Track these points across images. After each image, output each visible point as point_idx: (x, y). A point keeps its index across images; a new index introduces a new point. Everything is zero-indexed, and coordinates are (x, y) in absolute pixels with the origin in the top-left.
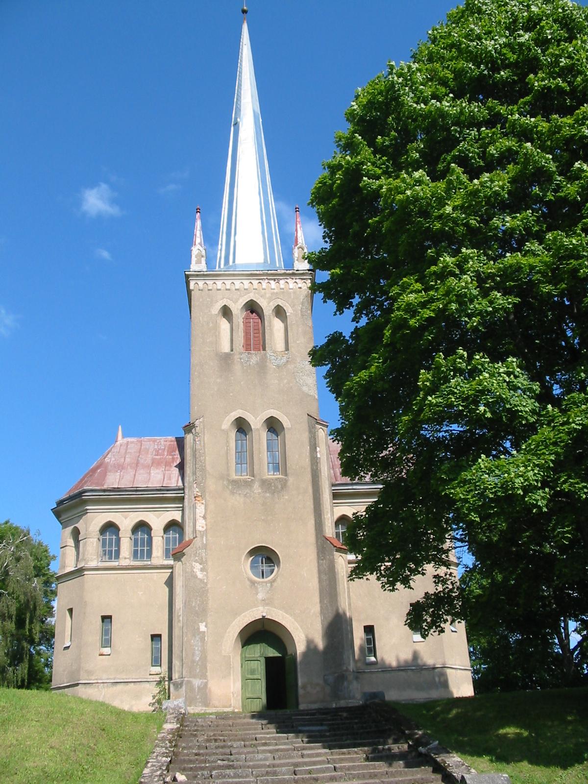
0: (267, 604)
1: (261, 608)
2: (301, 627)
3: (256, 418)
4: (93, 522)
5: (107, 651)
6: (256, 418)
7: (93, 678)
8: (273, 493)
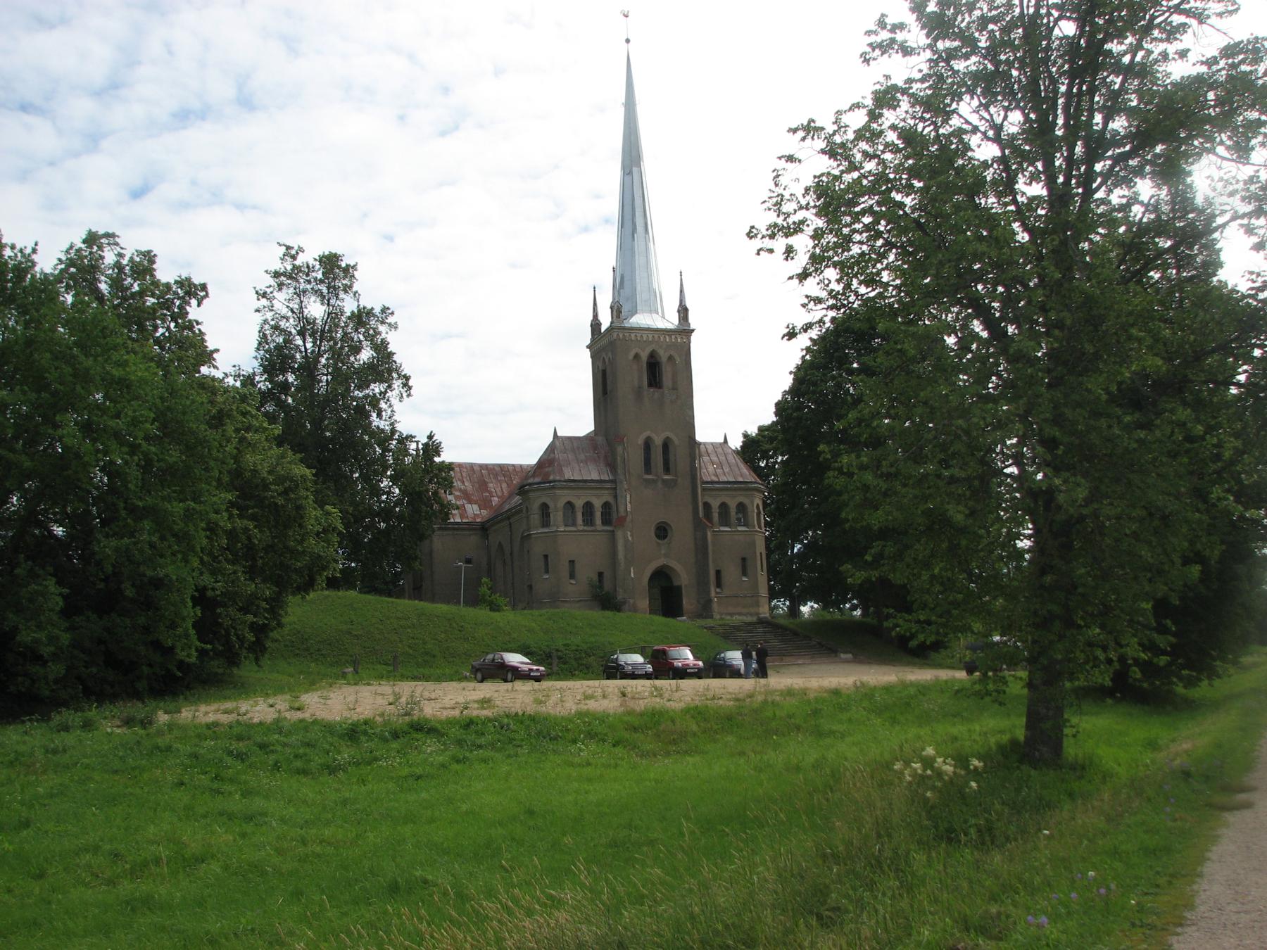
1: (663, 559)
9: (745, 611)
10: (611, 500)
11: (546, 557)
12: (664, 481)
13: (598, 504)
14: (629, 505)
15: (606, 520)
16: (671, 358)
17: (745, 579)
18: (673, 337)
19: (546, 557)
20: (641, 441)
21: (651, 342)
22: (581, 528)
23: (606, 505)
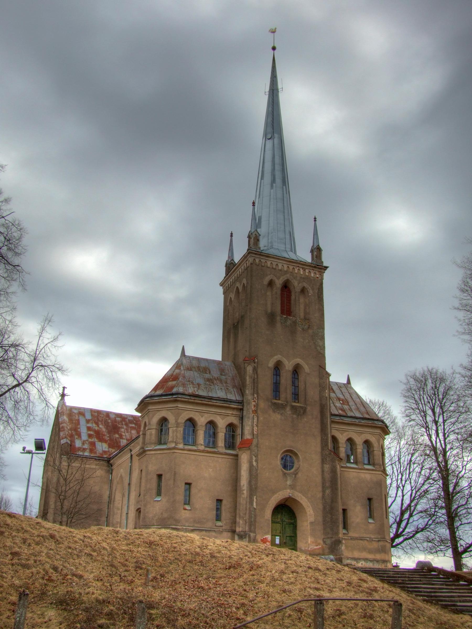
0: (292, 489)
1: (289, 491)
2: (311, 505)
3: (289, 363)
4: (181, 417)
5: (188, 507)
6: (289, 363)
7: (179, 524)
8: (298, 416)
9: (371, 556)
10: (235, 421)
11: (160, 476)
12: (293, 408)
13: (222, 423)
14: (255, 428)
15: (230, 445)
16: (303, 291)
17: (371, 521)
18: (307, 271)
19: (160, 476)
20: (271, 364)
21: (286, 272)
22: (202, 448)
23: (231, 426)
